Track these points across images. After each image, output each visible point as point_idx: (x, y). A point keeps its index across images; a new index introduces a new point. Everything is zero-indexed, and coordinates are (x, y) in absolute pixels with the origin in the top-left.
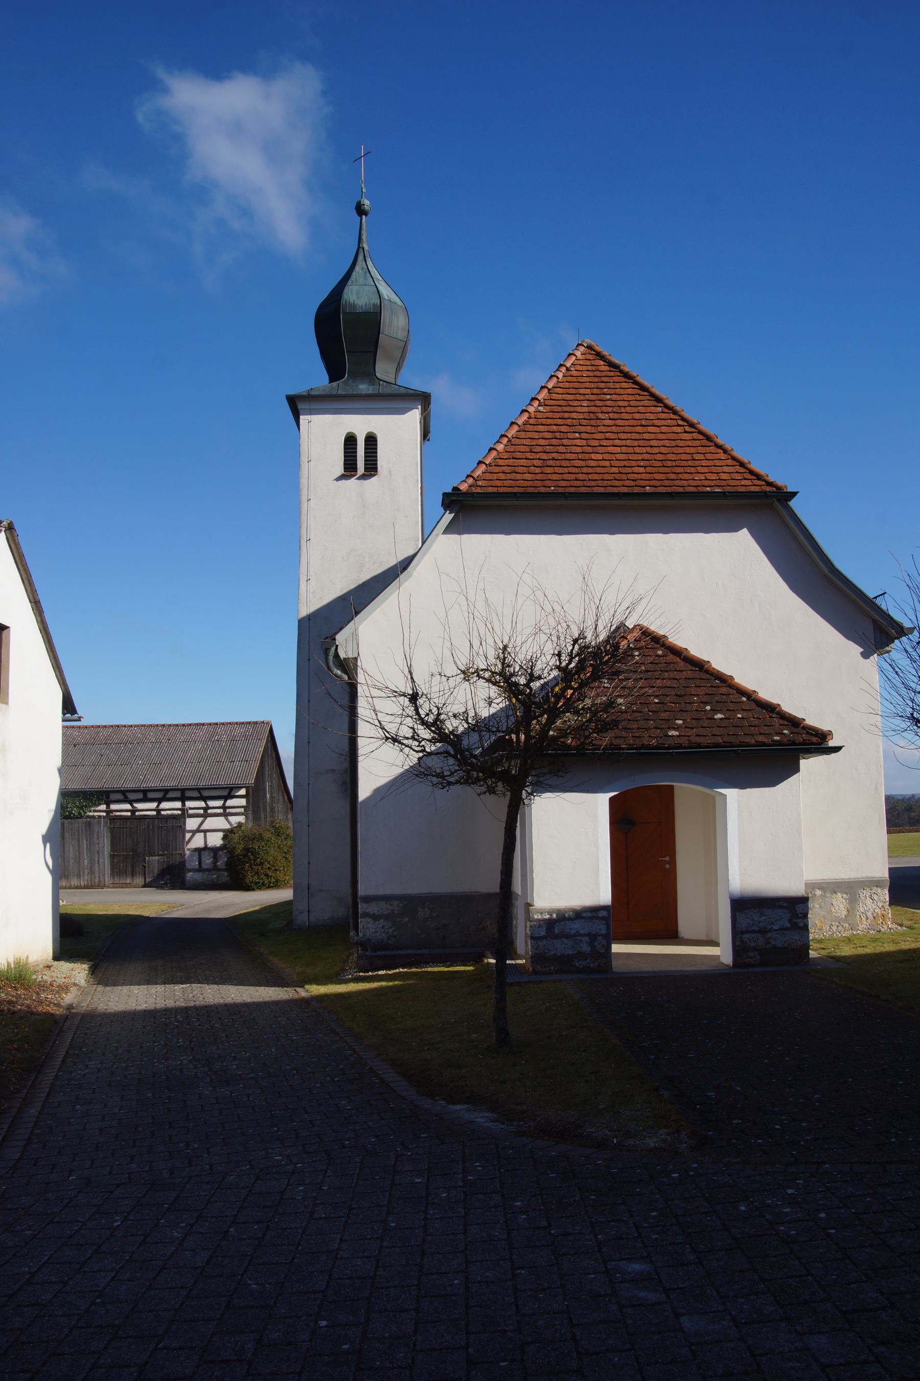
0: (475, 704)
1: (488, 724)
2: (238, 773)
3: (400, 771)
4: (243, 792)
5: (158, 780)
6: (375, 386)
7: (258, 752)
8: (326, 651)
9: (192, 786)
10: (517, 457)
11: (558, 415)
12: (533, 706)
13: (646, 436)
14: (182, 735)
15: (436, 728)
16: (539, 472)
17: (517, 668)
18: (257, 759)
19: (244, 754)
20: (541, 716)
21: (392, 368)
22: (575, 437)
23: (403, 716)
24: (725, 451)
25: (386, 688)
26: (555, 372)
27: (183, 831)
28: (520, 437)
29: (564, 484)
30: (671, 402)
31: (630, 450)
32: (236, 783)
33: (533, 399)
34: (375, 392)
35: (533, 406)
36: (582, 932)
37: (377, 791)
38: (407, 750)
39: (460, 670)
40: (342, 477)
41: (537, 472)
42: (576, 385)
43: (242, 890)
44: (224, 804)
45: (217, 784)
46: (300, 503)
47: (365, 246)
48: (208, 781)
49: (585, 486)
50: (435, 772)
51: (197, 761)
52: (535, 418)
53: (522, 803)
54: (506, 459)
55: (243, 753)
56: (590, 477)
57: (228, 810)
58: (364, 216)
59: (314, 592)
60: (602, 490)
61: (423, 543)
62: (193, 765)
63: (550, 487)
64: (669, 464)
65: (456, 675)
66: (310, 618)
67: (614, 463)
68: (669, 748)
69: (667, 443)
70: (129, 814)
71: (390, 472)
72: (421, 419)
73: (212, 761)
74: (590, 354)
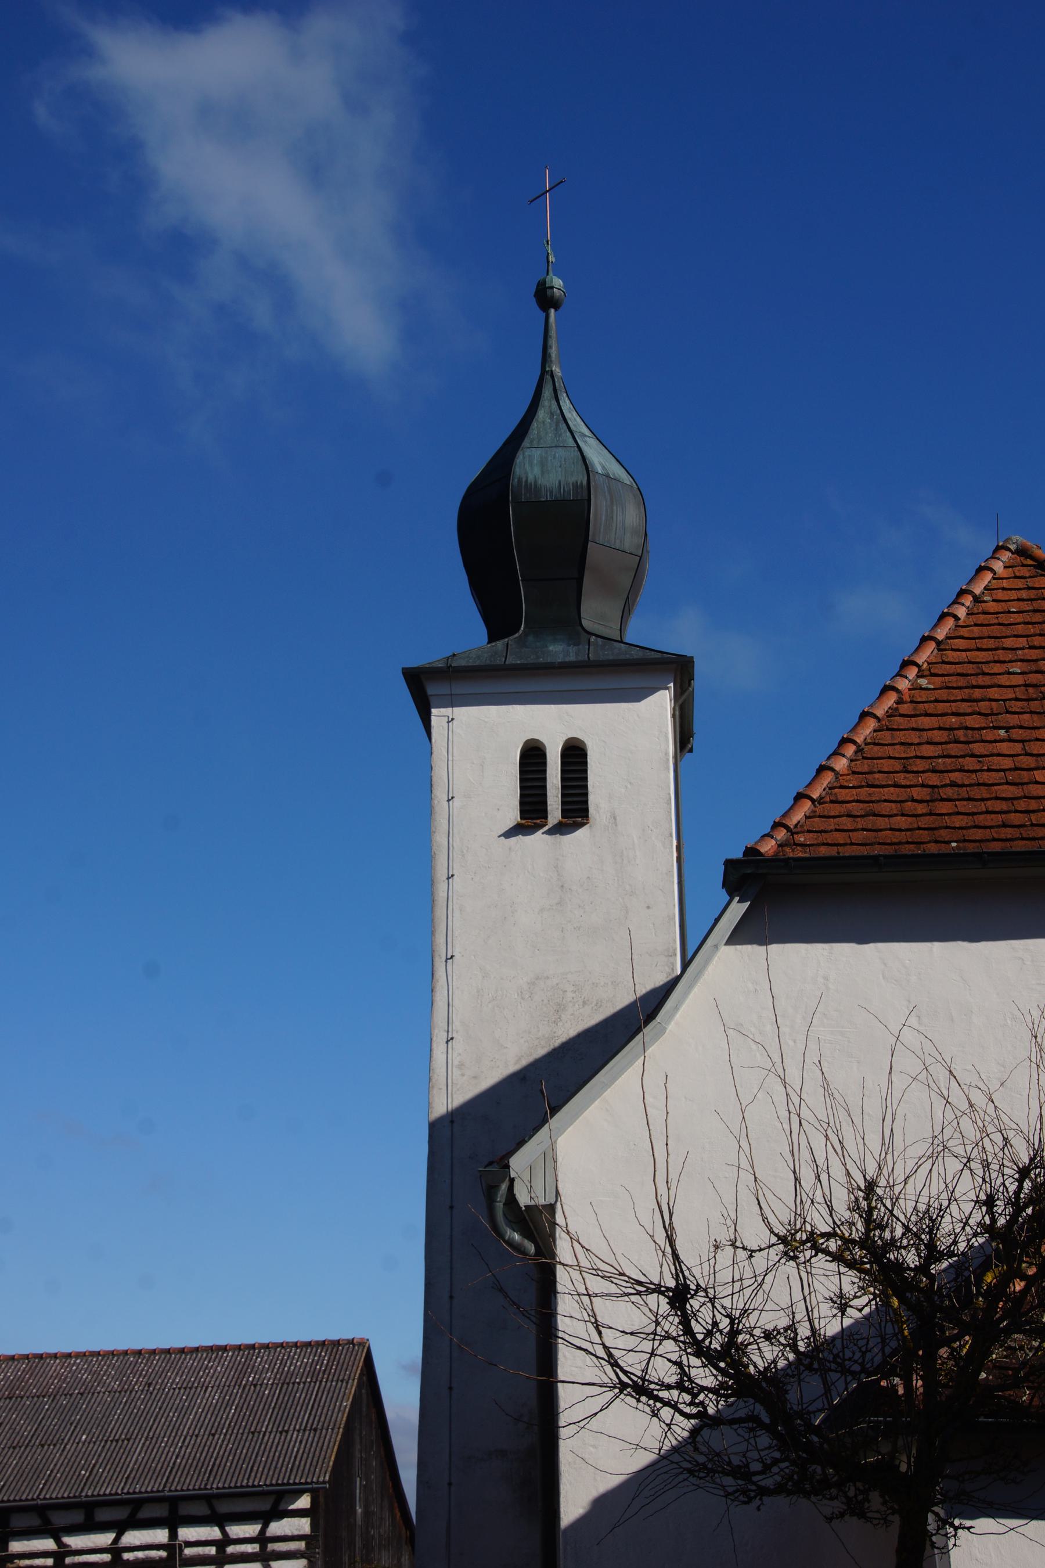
0: (810, 1309)
1: (841, 1354)
2: (296, 1457)
3: (645, 1459)
4: (304, 1502)
5: (120, 1477)
6: (581, 647)
7: (339, 1410)
8: (490, 1192)
9: (194, 1489)
10: (877, 783)
11: (958, 694)
12: (938, 1315)
14: (177, 1374)
15: (727, 1364)
16: (924, 811)
17: (899, 1231)
18: (337, 1426)
19: (310, 1414)
20: (958, 1337)
22: (998, 738)
23: (657, 1337)
25: (621, 1274)
26: (949, 606)
28: (882, 742)
29: (979, 834)
32: (291, 1481)
33: (906, 664)
34: (580, 658)
35: (906, 677)
37: (601, 1503)
38: (666, 1413)
39: (776, 1235)
40: (517, 830)
41: (920, 812)
42: (996, 631)
44: (263, 1531)
45: (250, 1484)
46: (432, 883)
47: (556, 369)
48: (229, 1477)
49: (1023, 839)
50: (729, 1463)
51: (207, 1433)
52: (912, 702)
53: (928, 1543)
54: (853, 787)
55: (308, 1412)
57: (271, 1547)
58: (552, 311)
59: (461, 1065)
61: (685, 965)
62: (199, 1441)
63: (949, 842)
65: (769, 1247)
66: (455, 1118)
71: (615, 818)
72: (674, 709)
73: (241, 1431)
74: (1023, 565)
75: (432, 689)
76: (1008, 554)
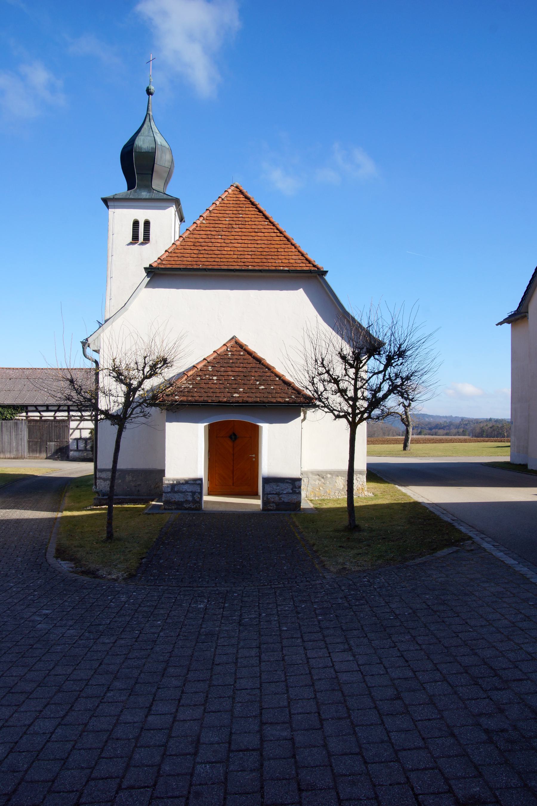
11: (212, 225)
13: (256, 238)
21: (162, 183)
24: (295, 248)
27: (68, 427)
30: (273, 220)
31: (246, 245)
36: (188, 490)
40: (131, 244)
43: (210, 460)
46: (108, 257)
56: (222, 260)
60: (226, 267)
64: (265, 253)
67: (235, 253)
68: (232, 403)
69: (266, 242)
70: (39, 418)
75: (109, 204)
76: (234, 187)
